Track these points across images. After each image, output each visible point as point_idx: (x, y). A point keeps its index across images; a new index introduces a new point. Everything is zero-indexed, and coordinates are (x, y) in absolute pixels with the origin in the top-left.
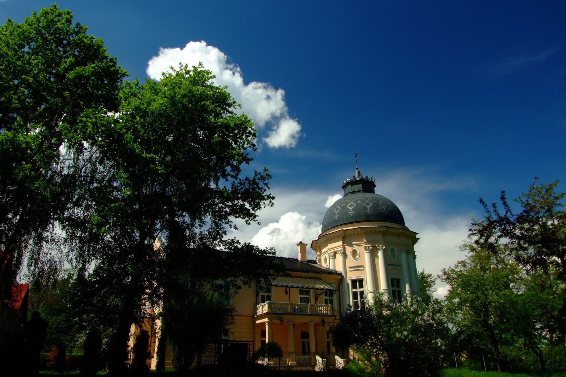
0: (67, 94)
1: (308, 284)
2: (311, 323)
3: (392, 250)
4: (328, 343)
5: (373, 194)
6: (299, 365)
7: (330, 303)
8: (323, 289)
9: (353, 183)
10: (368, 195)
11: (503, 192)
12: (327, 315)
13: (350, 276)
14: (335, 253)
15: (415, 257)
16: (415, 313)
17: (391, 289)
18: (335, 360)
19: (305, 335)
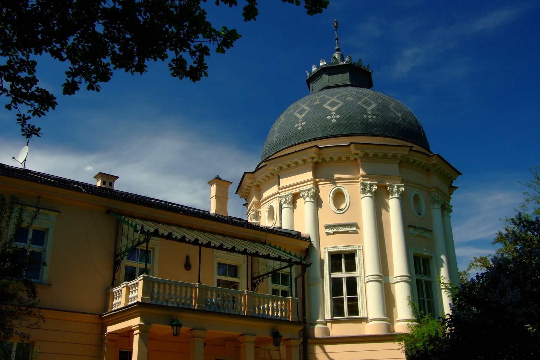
0: (24, 308)
2: (247, 338)
11: (336, 22)
12: (283, 321)
13: (327, 245)
14: (296, 196)
17: (415, 277)
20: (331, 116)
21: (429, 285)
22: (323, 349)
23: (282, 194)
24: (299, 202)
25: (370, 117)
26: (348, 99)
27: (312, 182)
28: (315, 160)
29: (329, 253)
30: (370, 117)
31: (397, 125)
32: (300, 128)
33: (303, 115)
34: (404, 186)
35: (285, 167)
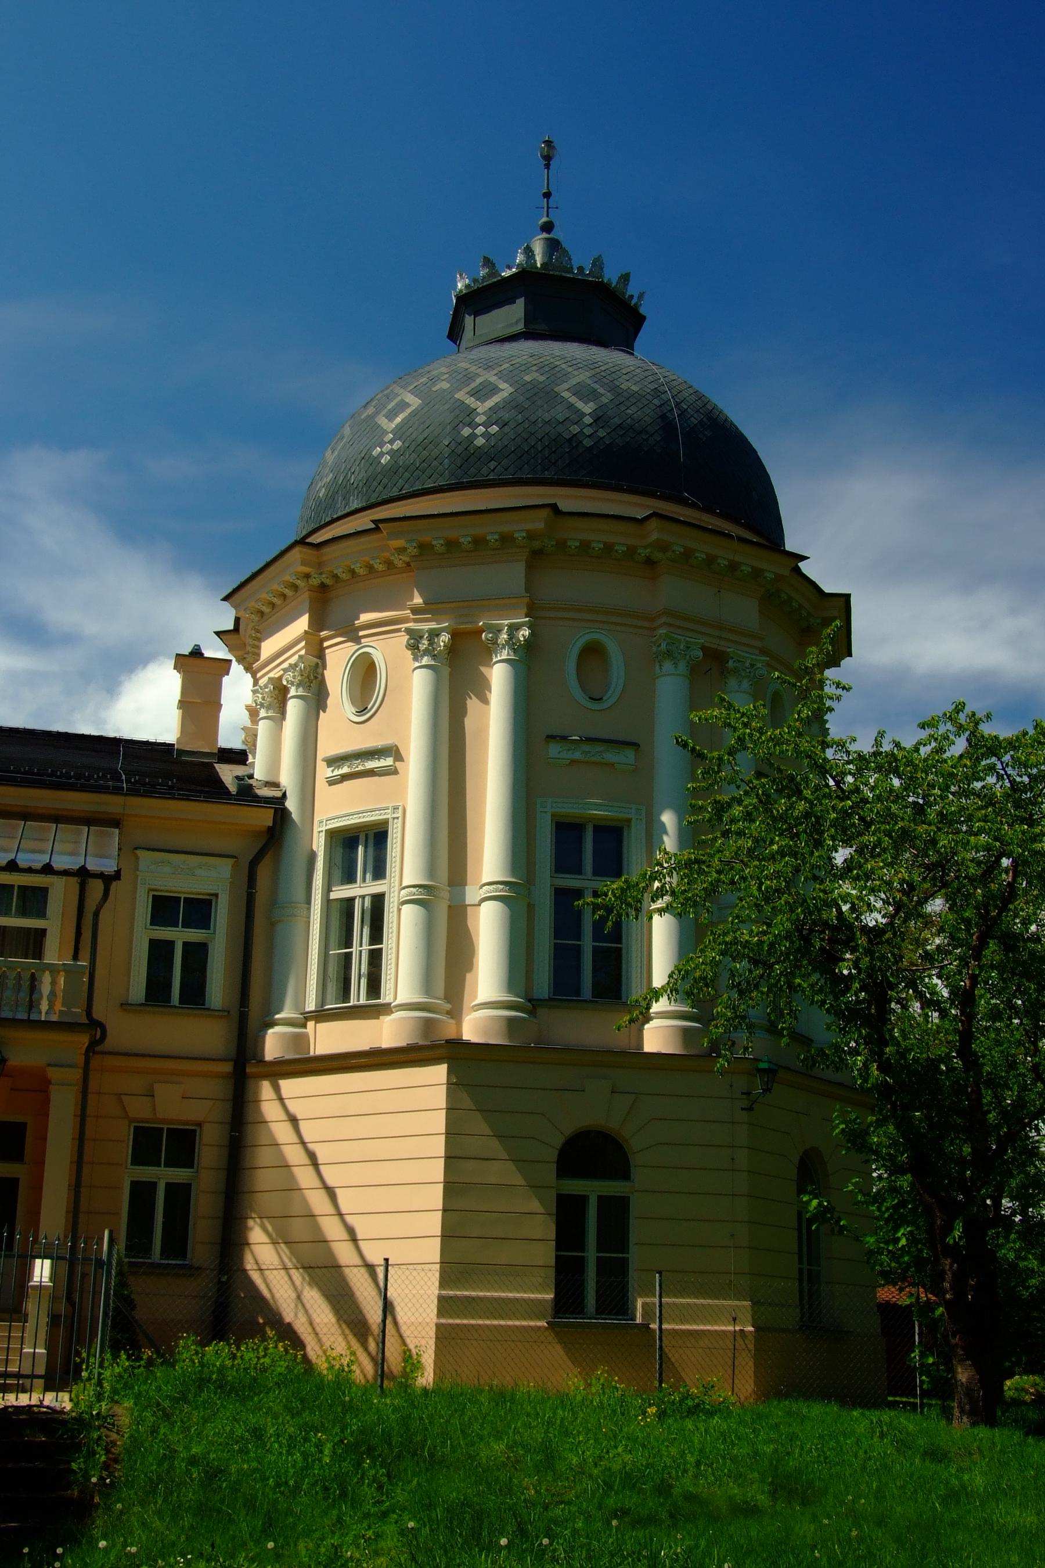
3: (592, 652)
11: (548, 143)
13: (336, 807)
22: (277, 1089)
27: (303, 644)
28: (315, 582)
31: (570, 440)
35: (266, 609)
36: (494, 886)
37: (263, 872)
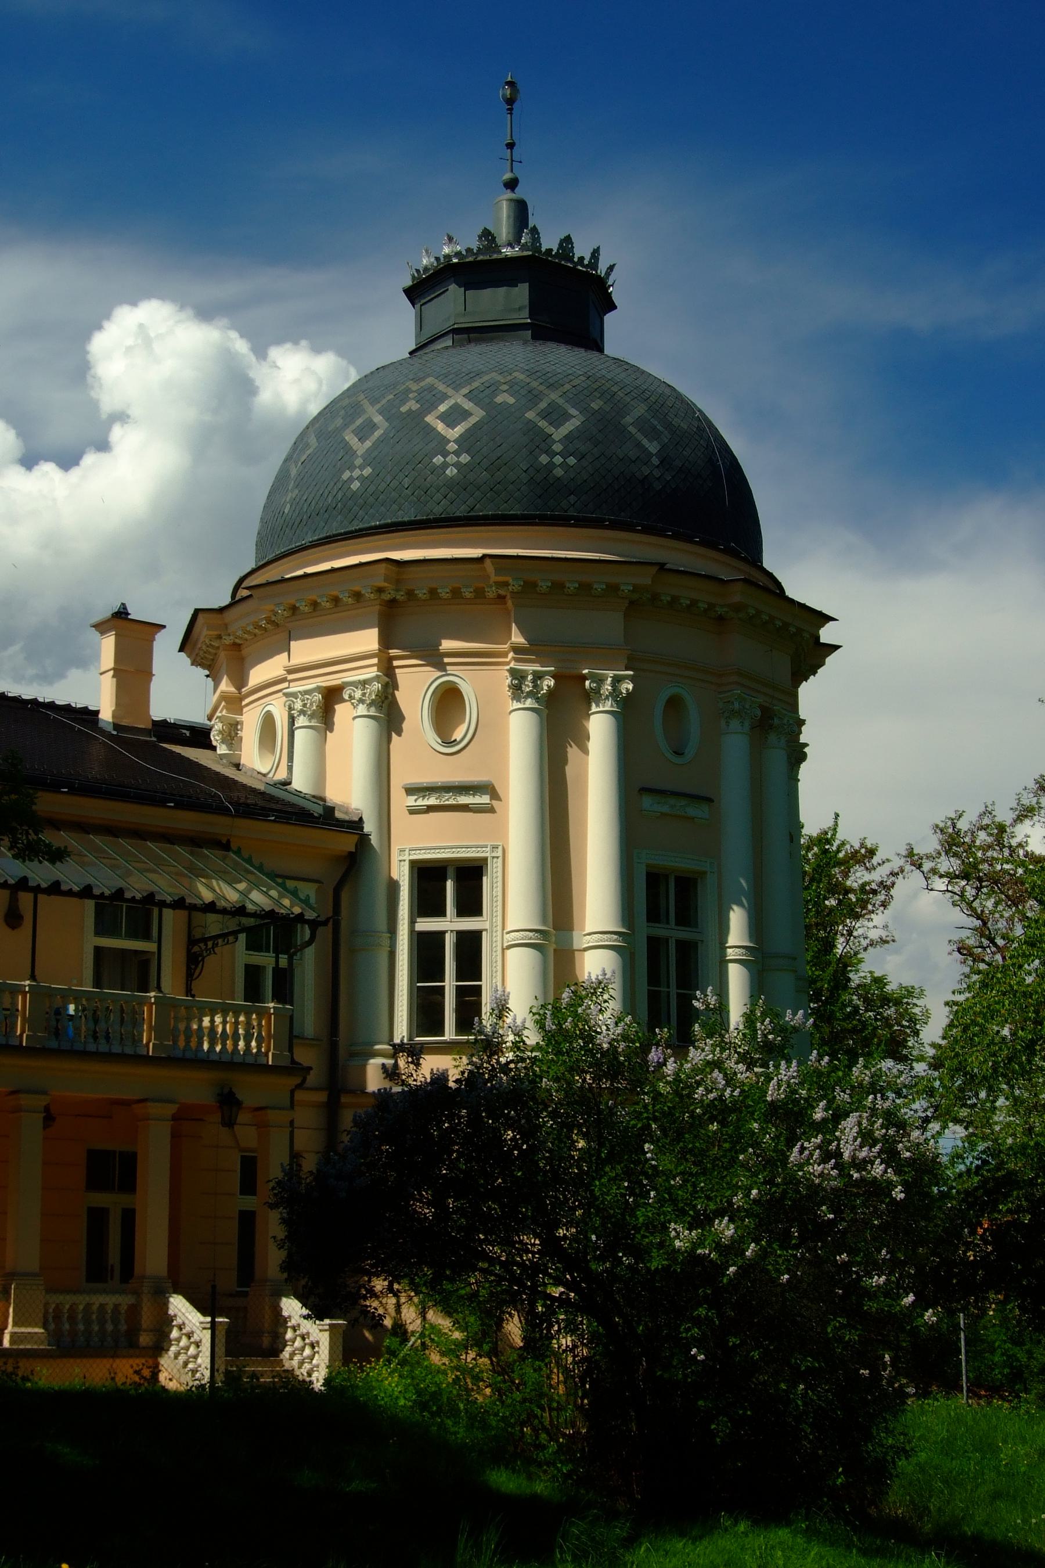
1: (145, 875)
3: (674, 704)
4: (247, 1221)
5: (594, 355)
6: (66, 1344)
7: (278, 997)
8: (240, 911)
9: (473, 272)
10: (563, 359)
11: (511, 84)
12: (253, 1066)
13: (413, 840)
14: (332, 696)
15: (797, 755)
16: (791, 1117)
17: (644, 929)
18: (280, 1321)
19: (113, 1170)
20: (445, 454)
21: (688, 952)
23: (295, 688)
24: (342, 712)
25: (558, 460)
26: (499, 399)
27: (375, 661)
28: (386, 597)
29: (413, 863)
30: (558, 460)
32: (355, 485)
33: (368, 444)
34: (632, 679)
35: (304, 608)
36: (609, 936)
37: (345, 896)
